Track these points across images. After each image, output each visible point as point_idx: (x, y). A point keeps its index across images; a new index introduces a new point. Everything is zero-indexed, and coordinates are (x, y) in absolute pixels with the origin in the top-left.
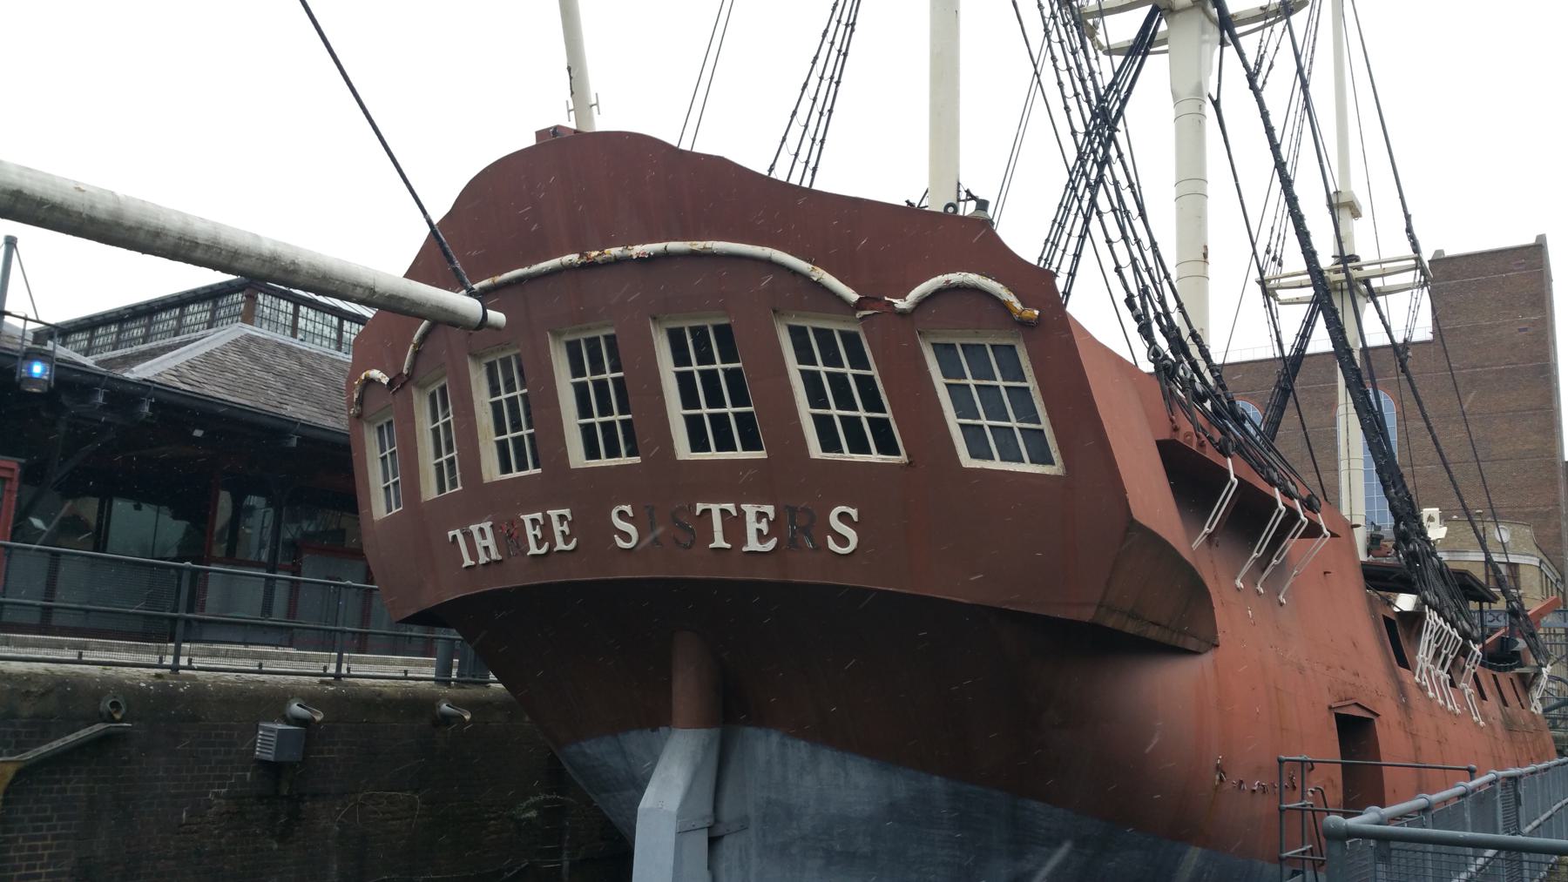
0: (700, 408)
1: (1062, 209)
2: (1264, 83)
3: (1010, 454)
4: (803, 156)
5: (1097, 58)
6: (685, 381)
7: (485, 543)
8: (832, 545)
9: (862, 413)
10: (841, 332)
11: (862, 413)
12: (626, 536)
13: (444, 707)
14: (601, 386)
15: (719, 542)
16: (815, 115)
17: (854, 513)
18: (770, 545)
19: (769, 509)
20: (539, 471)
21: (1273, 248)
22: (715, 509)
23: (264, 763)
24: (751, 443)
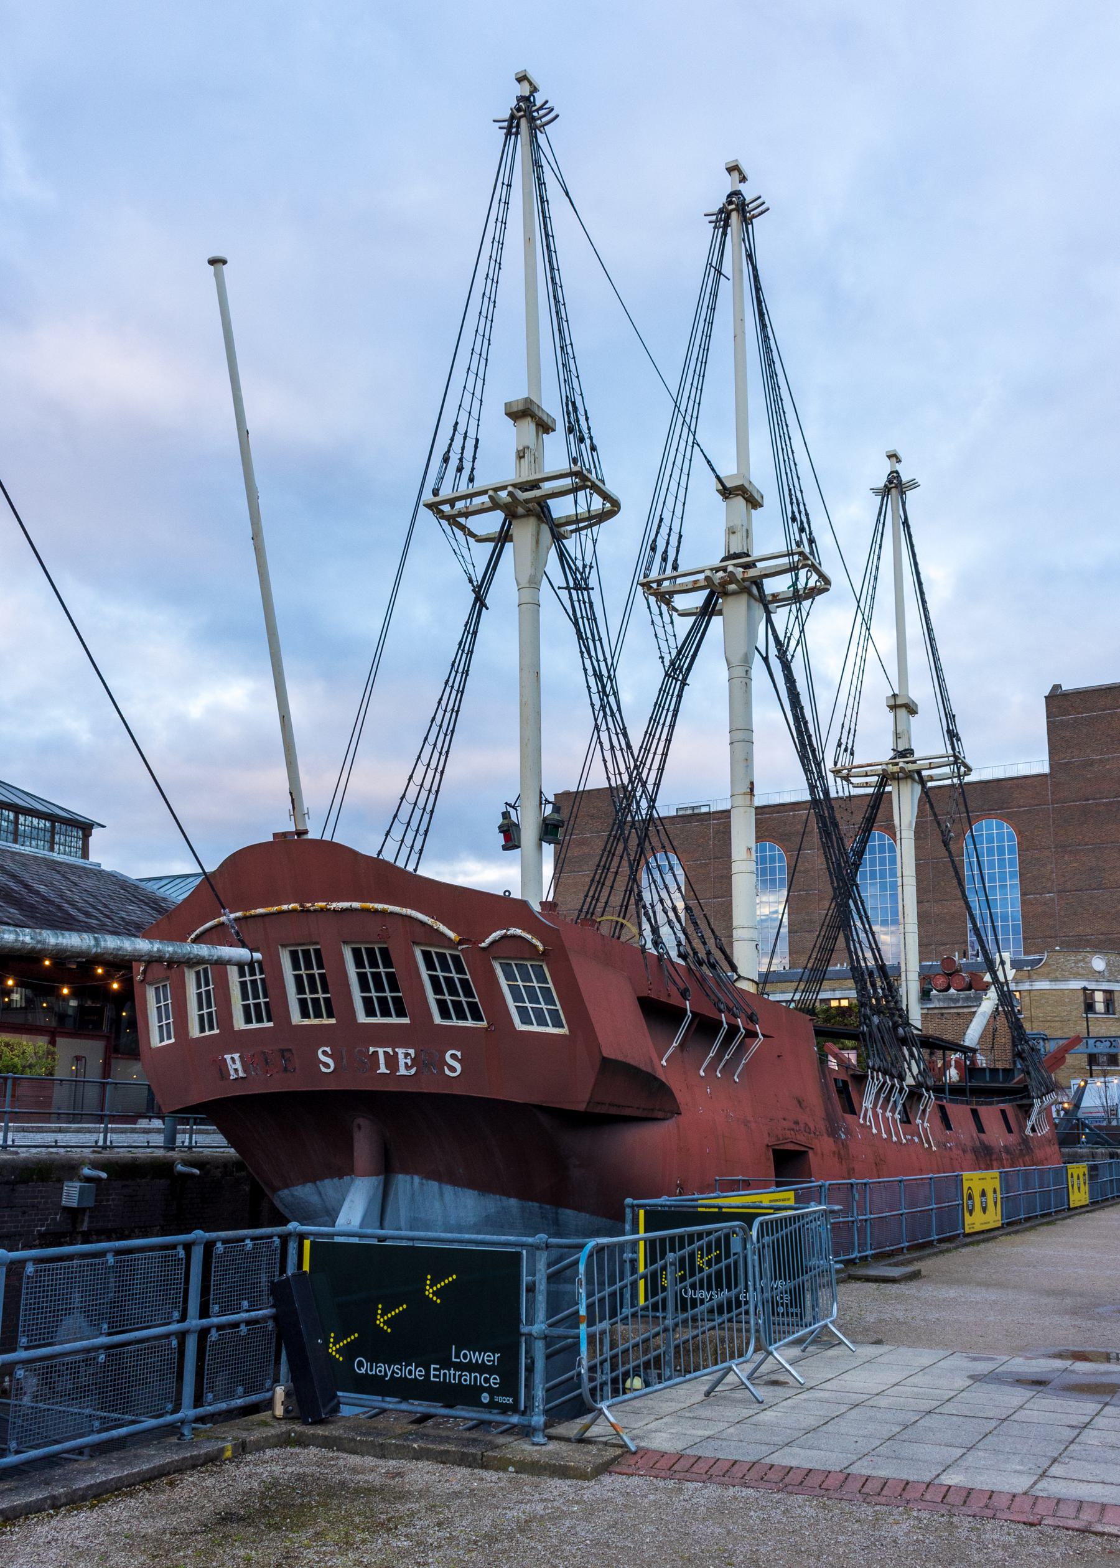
0: (370, 992)
1: (643, 750)
2: (793, 656)
3: (542, 1022)
4: (433, 765)
5: (672, 622)
6: (362, 978)
7: (234, 1066)
8: (447, 1072)
9: (463, 999)
10: (450, 954)
11: (463, 999)
12: (327, 1066)
13: (180, 1168)
14: (311, 977)
15: (383, 1069)
16: (442, 736)
17: (459, 1054)
18: (413, 1071)
19: (412, 1051)
20: (271, 1024)
21: (844, 741)
22: (381, 1051)
23: (68, 1210)
24: (401, 1013)
